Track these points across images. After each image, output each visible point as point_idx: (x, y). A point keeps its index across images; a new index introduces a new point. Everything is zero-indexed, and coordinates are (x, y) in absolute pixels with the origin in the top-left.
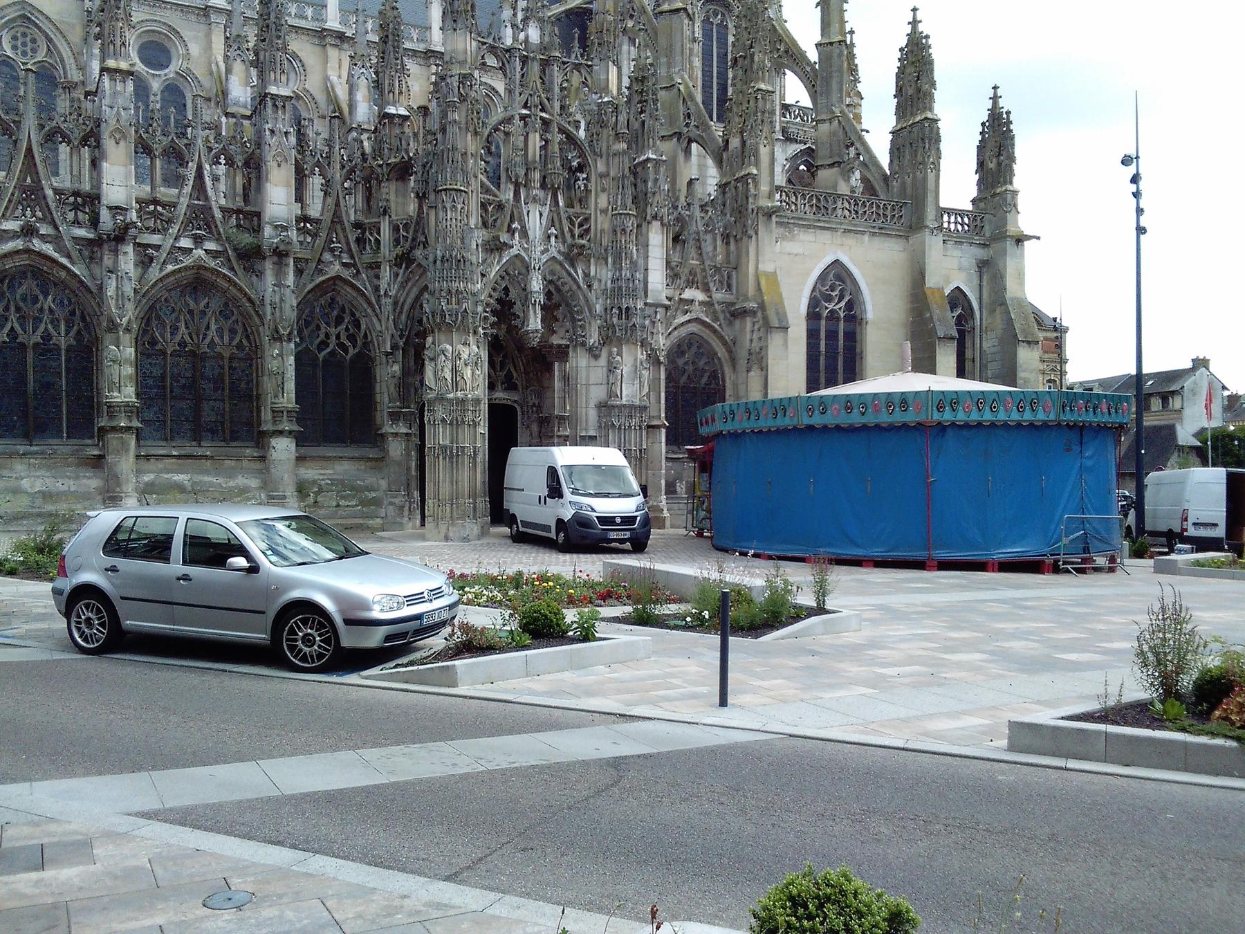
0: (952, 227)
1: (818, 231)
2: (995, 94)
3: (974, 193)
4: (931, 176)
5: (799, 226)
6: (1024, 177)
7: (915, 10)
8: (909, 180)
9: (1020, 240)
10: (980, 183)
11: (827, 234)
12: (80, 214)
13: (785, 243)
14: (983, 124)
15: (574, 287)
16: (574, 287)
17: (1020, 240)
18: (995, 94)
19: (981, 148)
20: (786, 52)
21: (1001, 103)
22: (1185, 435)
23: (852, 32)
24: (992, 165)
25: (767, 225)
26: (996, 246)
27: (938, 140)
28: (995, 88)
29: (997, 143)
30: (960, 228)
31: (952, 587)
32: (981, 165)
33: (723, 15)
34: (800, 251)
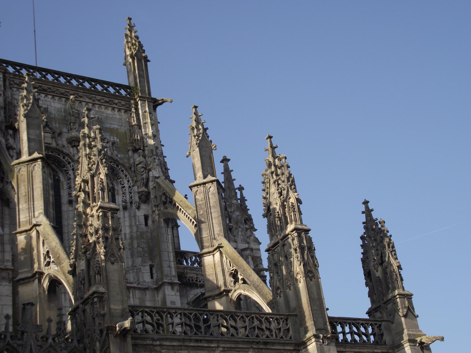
0: (349, 337)
2: (367, 207)
3: (367, 304)
7: (366, 203)
10: (370, 295)
12: (81, 209)
14: (362, 238)
18: (367, 207)
19: (364, 261)
21: (375, 215)
22: (146, 190)
23: (241, 189)
24: (379, 274)
28: (366, 203)
30: (357, 338)
31: (63, 186)
32: (368, 275)
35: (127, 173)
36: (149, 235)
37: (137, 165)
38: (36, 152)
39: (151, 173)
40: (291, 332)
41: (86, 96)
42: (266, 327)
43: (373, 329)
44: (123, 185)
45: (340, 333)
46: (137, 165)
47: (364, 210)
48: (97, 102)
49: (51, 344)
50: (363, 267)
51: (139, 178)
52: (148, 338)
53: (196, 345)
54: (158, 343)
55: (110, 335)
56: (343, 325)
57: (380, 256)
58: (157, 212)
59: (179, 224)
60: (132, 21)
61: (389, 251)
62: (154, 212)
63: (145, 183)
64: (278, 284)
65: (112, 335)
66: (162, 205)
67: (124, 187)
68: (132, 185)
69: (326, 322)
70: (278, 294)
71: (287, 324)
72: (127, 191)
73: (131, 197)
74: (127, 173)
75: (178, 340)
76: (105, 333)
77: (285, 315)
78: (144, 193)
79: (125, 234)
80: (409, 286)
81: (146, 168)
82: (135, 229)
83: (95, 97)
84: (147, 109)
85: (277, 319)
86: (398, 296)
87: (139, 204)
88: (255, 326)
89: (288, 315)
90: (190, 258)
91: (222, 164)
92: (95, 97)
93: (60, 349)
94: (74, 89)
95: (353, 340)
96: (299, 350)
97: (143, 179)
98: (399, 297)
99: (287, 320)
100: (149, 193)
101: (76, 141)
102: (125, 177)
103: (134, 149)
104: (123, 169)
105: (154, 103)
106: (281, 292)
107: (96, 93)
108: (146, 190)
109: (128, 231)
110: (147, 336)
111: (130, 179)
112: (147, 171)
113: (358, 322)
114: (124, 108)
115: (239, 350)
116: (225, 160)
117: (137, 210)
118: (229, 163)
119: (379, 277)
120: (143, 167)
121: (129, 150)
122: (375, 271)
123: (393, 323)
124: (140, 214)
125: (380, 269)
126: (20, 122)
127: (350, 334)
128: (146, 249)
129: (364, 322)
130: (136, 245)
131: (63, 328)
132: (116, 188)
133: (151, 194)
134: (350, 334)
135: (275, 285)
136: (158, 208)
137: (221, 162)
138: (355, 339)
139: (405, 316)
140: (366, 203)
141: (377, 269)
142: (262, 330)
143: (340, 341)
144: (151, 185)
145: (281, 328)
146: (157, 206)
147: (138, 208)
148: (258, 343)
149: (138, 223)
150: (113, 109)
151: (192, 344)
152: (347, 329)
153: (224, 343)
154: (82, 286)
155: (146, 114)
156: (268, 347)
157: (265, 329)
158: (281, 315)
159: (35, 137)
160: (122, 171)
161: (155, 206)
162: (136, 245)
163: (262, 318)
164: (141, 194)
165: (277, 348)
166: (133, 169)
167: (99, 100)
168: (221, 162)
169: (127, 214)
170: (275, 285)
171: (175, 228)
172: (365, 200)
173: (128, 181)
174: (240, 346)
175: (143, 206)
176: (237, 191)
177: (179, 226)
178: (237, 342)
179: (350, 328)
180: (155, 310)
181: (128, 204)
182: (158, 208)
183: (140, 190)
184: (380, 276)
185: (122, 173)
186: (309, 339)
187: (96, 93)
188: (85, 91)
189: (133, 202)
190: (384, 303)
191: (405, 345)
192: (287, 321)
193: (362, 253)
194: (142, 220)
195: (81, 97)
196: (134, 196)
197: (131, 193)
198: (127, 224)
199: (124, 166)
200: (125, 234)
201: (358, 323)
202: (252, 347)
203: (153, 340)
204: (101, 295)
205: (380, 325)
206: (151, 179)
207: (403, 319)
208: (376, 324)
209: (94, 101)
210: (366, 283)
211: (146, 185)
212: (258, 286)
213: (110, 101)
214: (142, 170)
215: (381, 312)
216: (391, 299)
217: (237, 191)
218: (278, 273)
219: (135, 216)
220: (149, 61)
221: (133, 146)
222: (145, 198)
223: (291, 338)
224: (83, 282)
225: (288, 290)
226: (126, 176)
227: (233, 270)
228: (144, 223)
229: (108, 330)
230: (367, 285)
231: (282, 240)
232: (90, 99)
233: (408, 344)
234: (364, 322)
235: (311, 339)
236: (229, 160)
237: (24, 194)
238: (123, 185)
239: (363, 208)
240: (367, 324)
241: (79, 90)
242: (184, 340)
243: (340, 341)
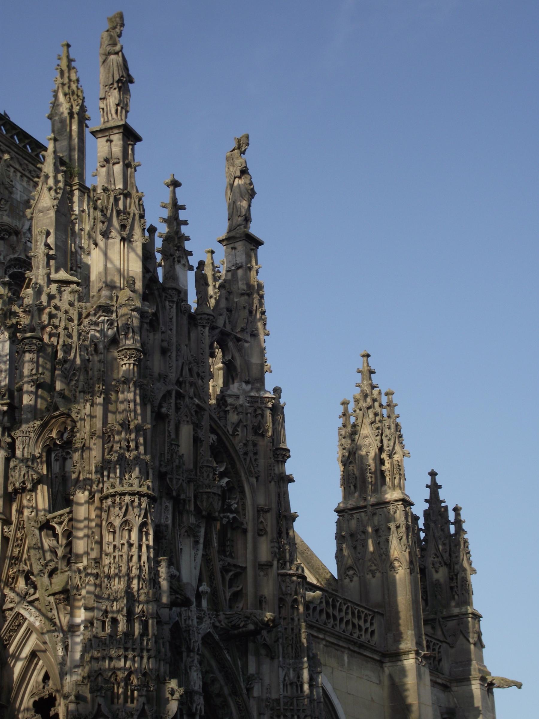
2: (434, 481)
15: (226, 691)
16: (226, 691)
18: (434, 481)
28: (433, 474)
38: (62, 269)
41: (18, 158)
47: (429, 483)
48: (27, 174)
60: (70, 49)
61: (464, 552)
69: (422, 635)
80: (479, 602)
84: (85, 207)
86: (471, 616)
92: (27, 165)
94: (8, 144)
98: (472, 618)
101: (8, 232)
107: (30, 160)
122: (433, 570)
123: (452, 647)
126: (36, 211)
139: (475, 644)
140: (433, 474)
155: (84, 214)
156: (362, 651)
167: (30, 172)
172: (433, 470)
174: (341, 643)
184: (442, 580)
186: (407, 653)
187: (30, 160)
188: (19, 152)
191: (473, 682)
202: (349, 649)
207: (472, 647)
209: (24, 170)
212: (303, 553)
225: (369, 576)
232: (21, 165)
233: (478, 682)
235: (408, 654)
239: (428, 480)
241: (13, 147)
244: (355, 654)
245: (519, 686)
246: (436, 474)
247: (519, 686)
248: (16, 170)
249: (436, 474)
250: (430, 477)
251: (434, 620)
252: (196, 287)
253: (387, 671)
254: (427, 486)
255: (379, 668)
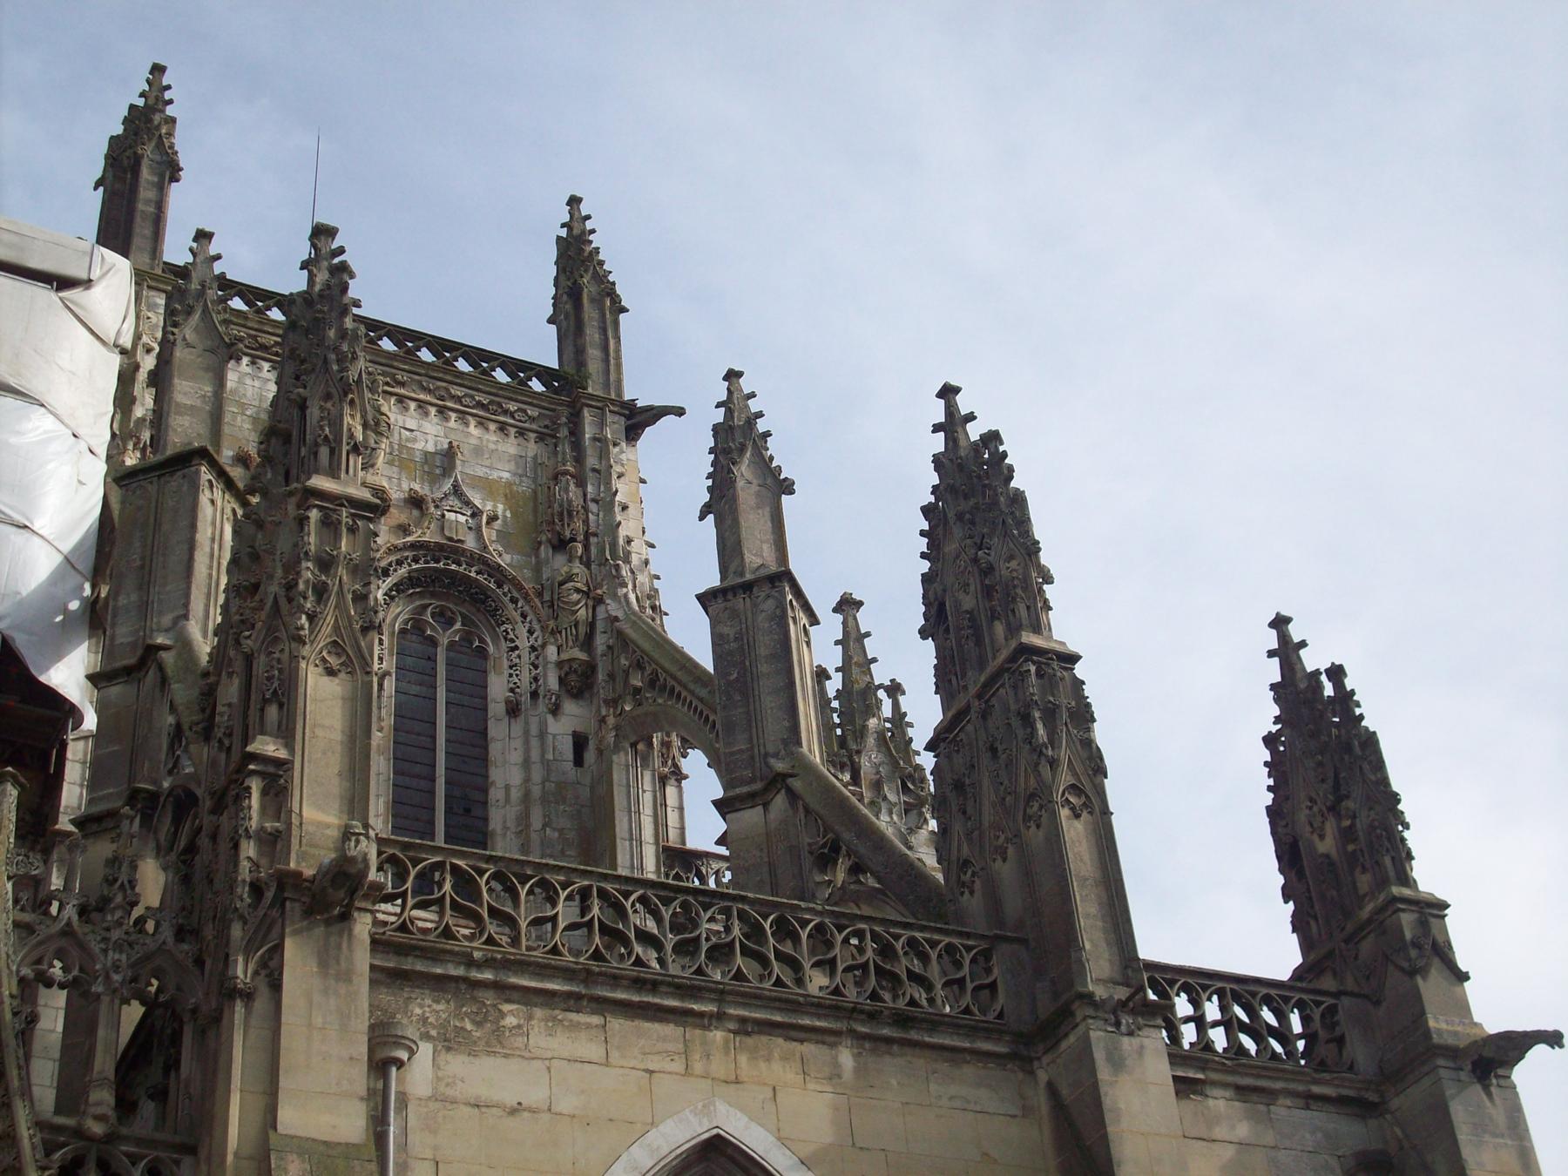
0: (1218, 1038)
1: (617, 1024)
2: (1284, 638)
4: (1075, 832)
5: (528, 997)
6: (1447, 849)
7: (1280, 623)
8: (1006, 871)
9: (1499, 1055)
10: (1298, 924)
11: (669, 1031)
13: (456, 1064)
17: (1499, 1055)
18: (1284, 638)
20: (652, 683)
21: (1313, 660)
22: (583, 656)
24: (1327, 845)
25: (330, 962)
26: (1406, 1101)
27: (1083, 715)
28: (1280, 623)
29: (1328, 780)
32: (1290, 854)
33: (466, 621)
34: (535, 1095)
35: (526, 608)
36: (585, 793)
37: (561, 584)
39: (601, 610)
40: (1001, 998)
42: (908, 970)
43: (1305, 1020)
44: (512, 641)
45: (1187, 1020)
46: (561, 584)
49: (69, 924)
50: (1274, 833)
51: (565, 621)
52: (450, 952)
53: (636, 998)
54: (488, 975)
55: (288, 904)
56: (1198, 994)
57: (1330, 782)
58: (611, 721)
59: (684, 771)
62: (603, 720)
63: (581, 637)
64: (965, 850)
65: (297, 905)
66: (629, 698)
67: (516, 648)
68: (540, 641)
70: (964, 884)
71: (988, 971)
72: (526, 658)
73: (536, 679)
74: (526, 608)
75: (568, 974)
76: (269, 895)
77: (983, 937)
78: (575, 666)
79: (507, 788)
81: (587, 594)
82: (537, 774)
83: (447, 390)
85: (950, 949)
87: (558, 697)
88: (867, 961)
89: (997, 937)
90: (717, 873)
91: (840, 617)
93: (103, 946)
95: (1236, 1049)
96: (1031, 1060)
97: (576, 626)
99: (986, 954)
100: (591, 668)
102: (519, 619)
103: (555, 541)
104: (516, 594)
105: (628, 418)
106: (973, 874)
107: (448, 378)
108: (583, 656)
109: (516, 777)
110: (450, 945)
111: (536, 626)
112: (590, 603)
113: (1252, 988)
114: (534, 427)
115: (802, 1035)
116: (847, 605)
117: (550, 718)
118: (861, 615)
119: (1327, 856)
120: (578, 591)
121: (540, 543)
123: (1377, 1003)
124: (561, 729)
125: (1330, 827)
127: (1222, 1029)
128: (571, 835)
129: (1273, 992)
130: (536, 821)
131: (123, 878)
132: (491, 649)
133: (600, 669)
134: (1222, 1029)
135: (954, 858)
136: (615, 708)
137: (835, 610)
138: (1241, 1045)
141: (1322, 829)
142: (894, 978)
143: (1186, 1046)
144: (600, 642)
145: (964, 978)
146: (613, 703)
147: (555, 710)
148: (872, 1016)
149: (550, 757)
150: (502, 428)
151: (620, 995)
152: (1212, 1011)
153: (745, 1005)
154: (223, 756)
156: (914, 1035)
157: (904, 977)
158: (968, 935)
159: (198, 403)
160: (514, 601)
161: (605, 701)
162: (536, 821)
163: (897, 937)
164: (566, 668)
165: (947, 1041)
166: (547, 597)
167: (458, 400)
168: (835, 610)
169: (517, 727)
170: (954, 858)
171: (672, 781)
173: (531, 632)
175: (570, 707)
176: (881, 694)
177: (686, 777)
178: (793, 1006)
179: (1223, 1008)
180: (492, 869)
181: (525, 699)
182: (615, 708)
183: (565, 656)
184: (1334, 853)
185: (511, 606)
189: (541, 692)
190: (1346, 941)
192: (988, 959)
193: (1270, 788)
194: (567, 747)
195: (402, 384)
196: (545, 676)
197: (536, 667)
198: (516, 757)
199: (520, 587)
200: (507, 788)
201: (1253, 995)
202: (853, 1033)
203: (470, 963)
204: (271, 769)
205: (1332, 1010)
206: (600, 626)
208: (1318, 1004)
210: (1284, 888)
211: (587, 643)
213: (491, 402)
214: (575, 597)
215: (1335, 974)
216: (1369, 921)
217: (881, 694)
218: (964, 813)
219: (542, 734)
220: (624, 310)
221: (552, 531)
222: (578, 682)
223: (1000, 1016)
224: (227, 742)
226: (524, 616)
227: (824, 846)
228: (570, 755)
229: (281, 887)
230: (1287, 895)
231: (979, 696)
234: (1273, 992)
236: (861, 603)
237: (138, 563)
238: (512, 641)
240: (1286, 1000)
242: (587, 976)
243: (1186, 1046)
244: (895, 1048)
245: (680, 412)
246: (1288, 620)
247: (680, 412)
248: (422, 405)
249: (1288, 620)
250: (1274, 632)
251: (1330, 955)
252: (1089, 705)
253: (1043, 1076)
254: (1271, 654)
255: (1021, 1075)
